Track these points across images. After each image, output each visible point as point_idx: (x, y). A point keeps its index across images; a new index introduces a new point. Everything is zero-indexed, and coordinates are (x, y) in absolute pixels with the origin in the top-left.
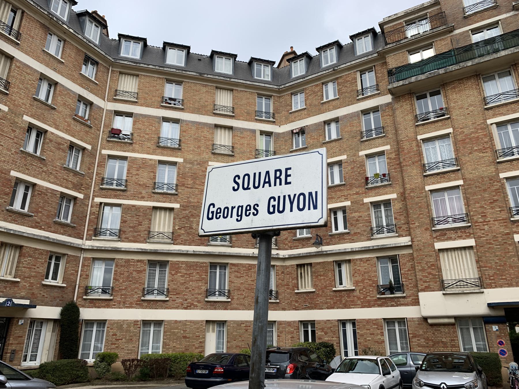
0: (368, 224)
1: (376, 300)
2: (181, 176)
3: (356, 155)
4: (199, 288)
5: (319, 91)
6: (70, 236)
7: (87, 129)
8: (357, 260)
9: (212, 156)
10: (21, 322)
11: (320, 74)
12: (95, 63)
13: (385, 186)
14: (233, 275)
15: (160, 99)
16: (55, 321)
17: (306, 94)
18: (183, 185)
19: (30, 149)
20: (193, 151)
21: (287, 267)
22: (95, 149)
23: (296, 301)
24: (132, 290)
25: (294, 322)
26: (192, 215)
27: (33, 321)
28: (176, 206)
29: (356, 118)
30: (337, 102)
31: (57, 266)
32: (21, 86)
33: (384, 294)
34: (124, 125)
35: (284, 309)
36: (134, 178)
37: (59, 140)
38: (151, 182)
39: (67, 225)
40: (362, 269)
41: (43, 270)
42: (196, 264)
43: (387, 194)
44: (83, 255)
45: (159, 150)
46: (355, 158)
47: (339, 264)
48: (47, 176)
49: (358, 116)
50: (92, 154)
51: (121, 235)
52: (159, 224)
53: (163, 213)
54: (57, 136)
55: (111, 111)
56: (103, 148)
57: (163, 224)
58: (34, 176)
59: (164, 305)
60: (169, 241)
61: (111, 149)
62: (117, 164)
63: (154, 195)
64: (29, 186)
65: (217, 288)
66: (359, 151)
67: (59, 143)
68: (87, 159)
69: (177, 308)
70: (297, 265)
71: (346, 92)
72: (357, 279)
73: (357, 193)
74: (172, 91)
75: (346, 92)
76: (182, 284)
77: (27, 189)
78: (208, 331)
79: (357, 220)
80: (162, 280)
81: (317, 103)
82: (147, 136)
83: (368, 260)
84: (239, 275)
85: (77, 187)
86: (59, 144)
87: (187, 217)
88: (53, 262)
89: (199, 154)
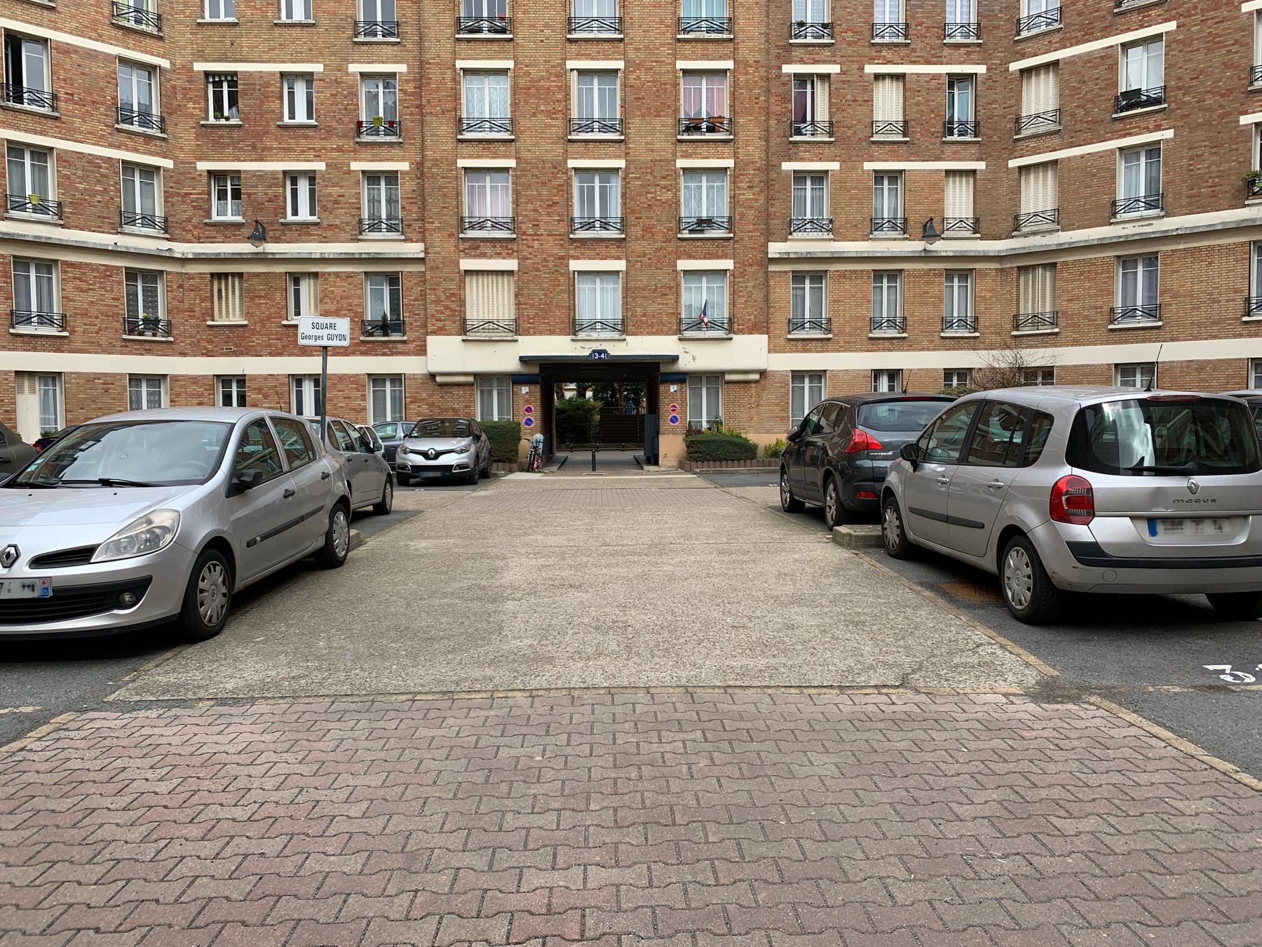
0: (354, 212)
3: (342, 69)
8: (329, 274)
21: (190, 277)
23: (210, 341)
25: (204, 377)
33: (371, 335)
35: (183, 354)
40: (338, 292)
65: (34, 308)
73: (339, 149)
78: (21, 391)
79: (336, 202)
83: (349, 276)
84: (84, 286)
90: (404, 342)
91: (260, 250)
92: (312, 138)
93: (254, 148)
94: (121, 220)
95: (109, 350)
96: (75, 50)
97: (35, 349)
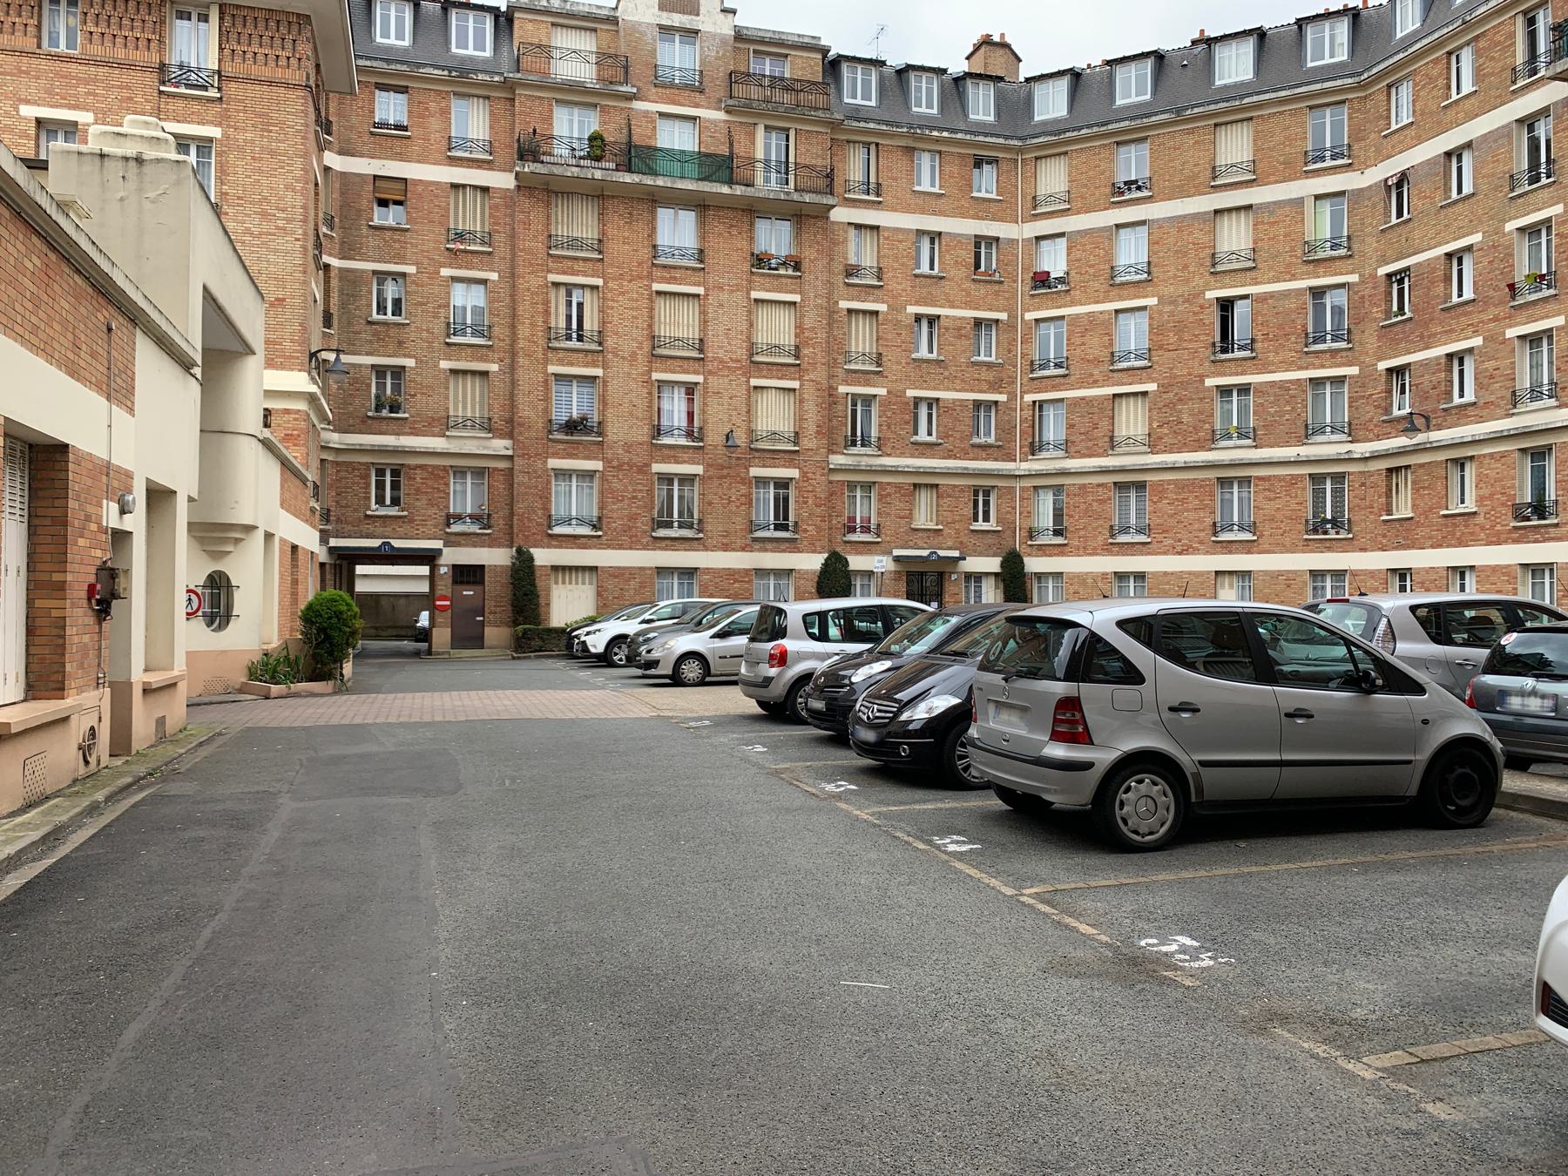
0: (1509, 384)
1: (1510, 532)
2: (1156, 330)
3: (1499, 231)
4: (1200, 521)
5: (1440, 75)
6: (996, 460)
7: (997, 287)
8: (1484, 456)
9: (1212, 279)
10: (954, 577)
11: (1436, 35)
12: (993, 161)
13: (1545, 300)
14: (1261, 496)
15: (1108, 190)
16: (996, 575)
17: (1415, 85)
18: (1161, 347)
19: (923, 352)
20: (1175, 276)
21: (1371, 474)
22: (1013, 316)
23: (1384, 536)
24: (1095, 529)
25: (1379, 571)
26: (1180, 400)
27: (968, 576)
28: (1151, 387)
29: (1505, 141)
30: (1472, 100)
31: (986, 503)
32: (896, 265)
33: (1528, 519)
34: (1054, 261)
35: (1363, 550)
36: (1078, 351)
37: (958, 323)
38: (1106, 352)
39: (990, 446)
40: (1492, 474)
41: (969, 511)
42: (1193, 482)
43: (1547, 317)
44: (1018, 485)
45: (1115, 292)
46: (1496, 237)
47: (1460, 463)
48: (949, 382)
49: (1509, 136)
50: (1011, 326)
51: (1068, 447)
52: (1128, 421)
53: (1132, 400)
54: (955, 318)
55: (1029, 239)
56: (1024, 310)
57: (1132, 422)
58: (935, 389)
59: (1144, 549)
60: (1146, 449)
61: (1039, 309)
62: (1051, 330)
63: (1114, 375)
64: (932, 403)
65: (1236, 519)
66: (1505, 221)
67: (958, 328)
68: (1004, 337)
69: (1165, 553)
70: (1390, 470)
71: (1492, 74)
72: (1482, 492)
73: (1496, 319)
74: (1132, 163)
75: (1492, 74)
76: (1171, 516)
77: (930, 407)
78: (1223, 587)
79: (1492, 377)
80: (1140, 512)
81: (1434, 108)
82: (1092, 271)
83: (1503, 455)
84: (1272, 495)
85: (995, 387)
86: (959, 329)
87: (1170, 405)
88: (981, 499)
89: (1187, 281)
90: (1557, 525)
91: (1415, 441)
92: (1470, 313)
93: (1422, 337)
94: (1308, 433)
95: (1292, 549)
96: (1271, 295)
97: (1230, 552)
